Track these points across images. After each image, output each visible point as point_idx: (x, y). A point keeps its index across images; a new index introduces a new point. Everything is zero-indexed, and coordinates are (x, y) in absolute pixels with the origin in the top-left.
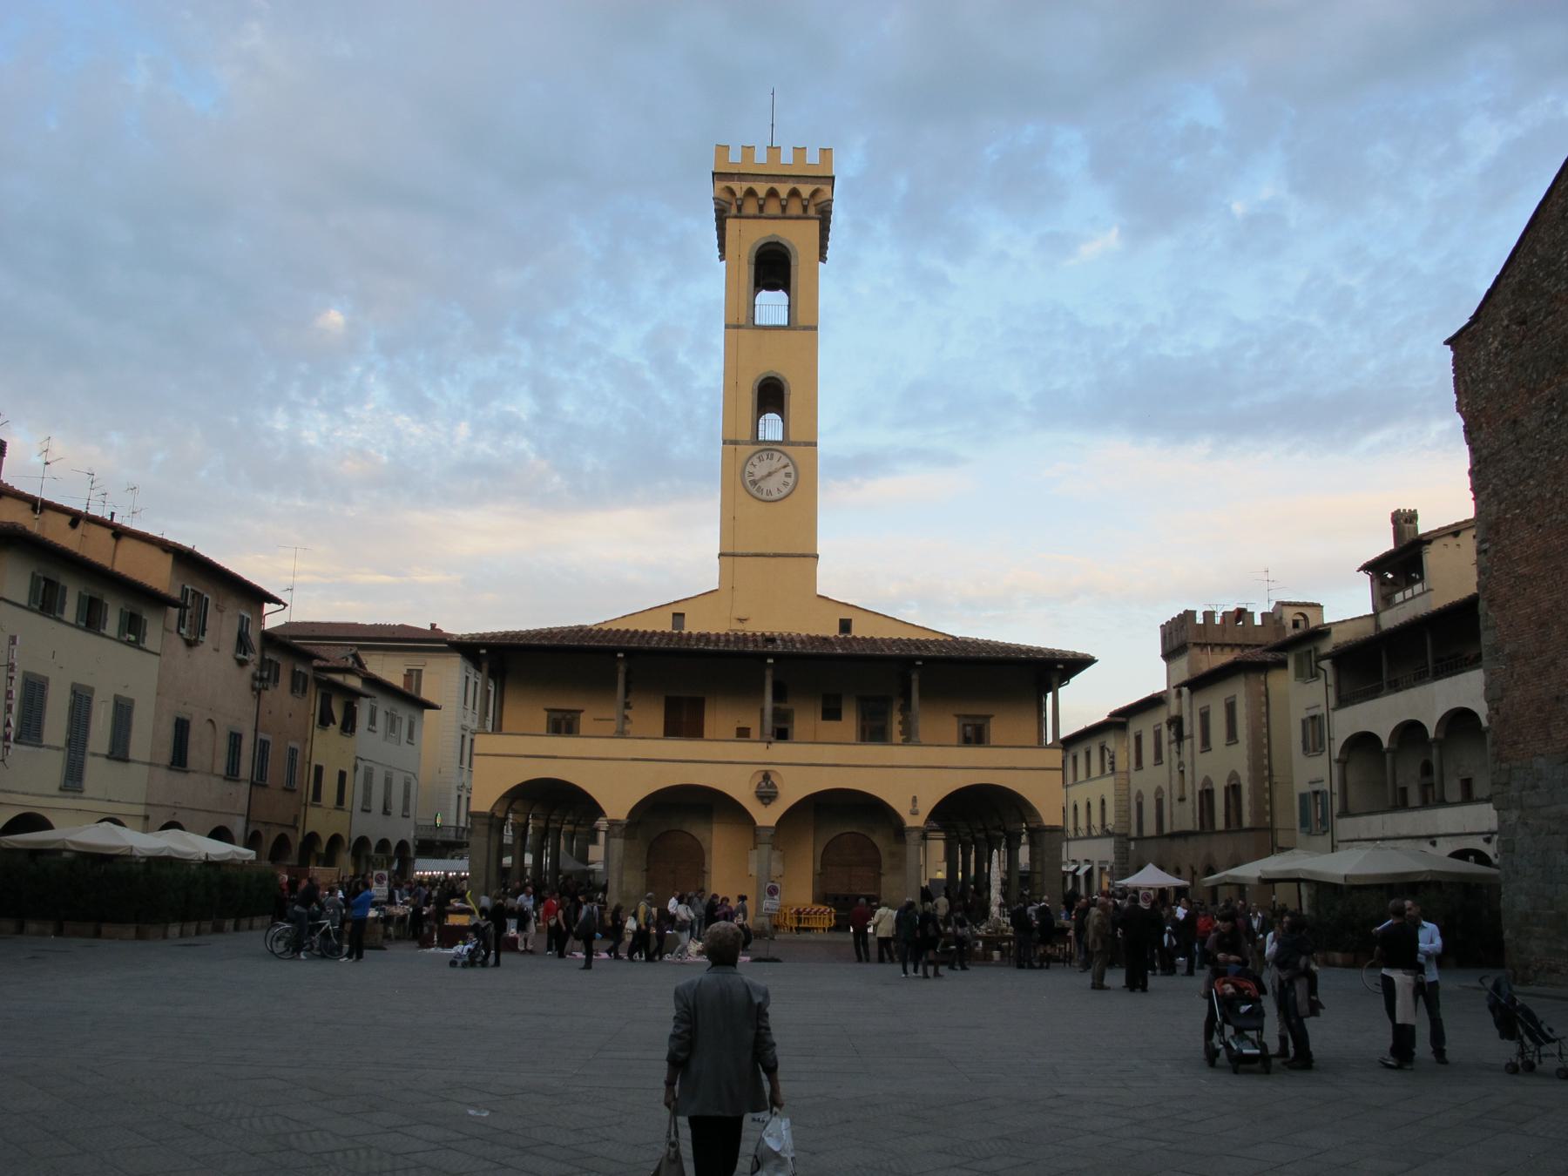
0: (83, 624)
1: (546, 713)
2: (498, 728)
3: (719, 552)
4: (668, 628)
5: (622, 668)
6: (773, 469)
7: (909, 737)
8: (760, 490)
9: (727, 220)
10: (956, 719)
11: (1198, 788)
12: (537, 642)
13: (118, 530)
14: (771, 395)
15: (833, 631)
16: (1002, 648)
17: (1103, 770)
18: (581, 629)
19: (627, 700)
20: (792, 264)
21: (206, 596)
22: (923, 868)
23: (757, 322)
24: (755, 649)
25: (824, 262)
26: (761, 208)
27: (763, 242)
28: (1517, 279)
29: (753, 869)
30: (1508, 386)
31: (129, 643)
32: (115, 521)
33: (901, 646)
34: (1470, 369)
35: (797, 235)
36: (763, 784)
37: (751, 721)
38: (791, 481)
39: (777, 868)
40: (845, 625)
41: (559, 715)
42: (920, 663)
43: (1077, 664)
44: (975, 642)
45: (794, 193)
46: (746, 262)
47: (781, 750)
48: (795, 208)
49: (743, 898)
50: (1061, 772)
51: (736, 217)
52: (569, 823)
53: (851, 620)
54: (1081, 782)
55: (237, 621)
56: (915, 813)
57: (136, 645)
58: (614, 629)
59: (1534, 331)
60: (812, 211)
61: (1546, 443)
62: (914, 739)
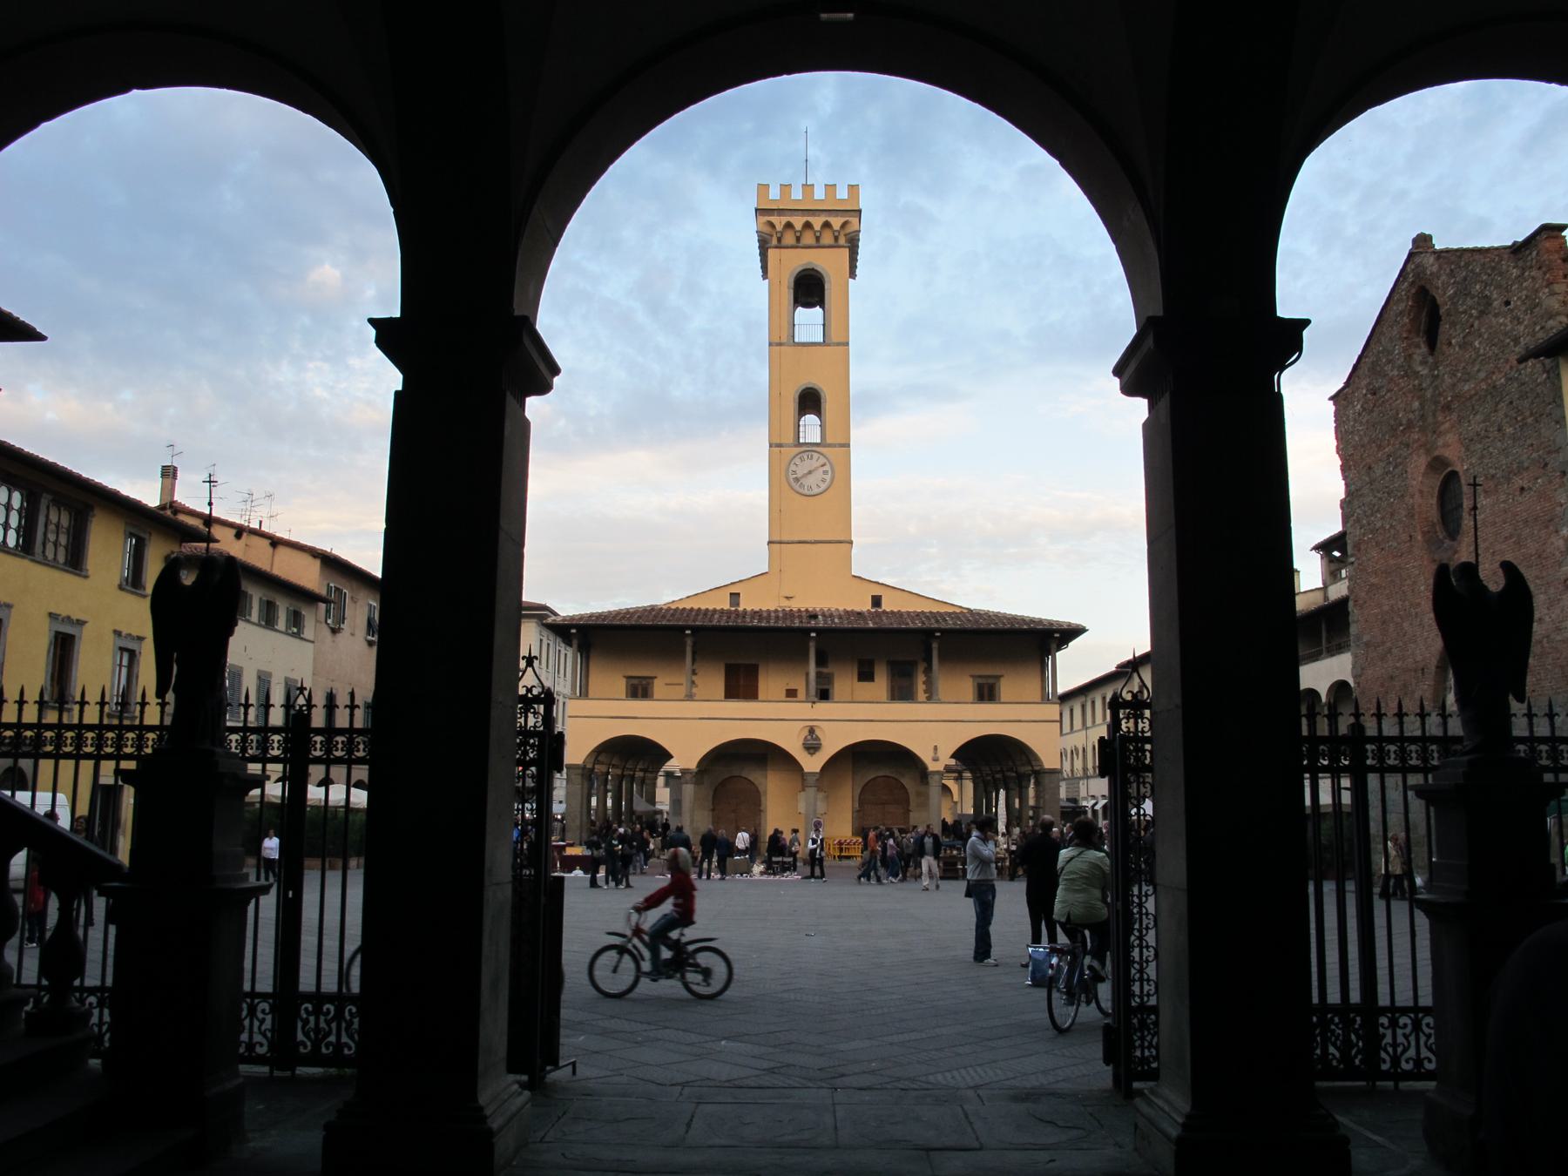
0: (263, 623)
2: (584, 694)
3: (768, 540)
4: (727, 606)
5: (689, 642)
6: (813, 468)
7: (931, 697)
8: (802, 486)
9: (769, 250)
10: (971, 679)
12: (618, 623)
13: (275, 540)
14: (809, 289)
15: (866, 606)
16: (1009, 619)
17: (1094, 722)
18: (652, 608)
19: (694, 667)
20: (826, 287)
21: (345, 591)
22: (959, 805)
23: (796, 340)
24: (801, 625)
25: (854, 279)
26: (798, 239)
27: (801, 269)
28: (1371, 360)
29: (802, 807)
30: (1366, 440)
31: (294, 635)
32: (263, 529)
33: (924, 619)
34: (1344, 422)
35: (828, 262)
36: (809, 737)
37: (798, 684)
38: (828, 477)
39: (821, 807)
40: (877, 601)
41: (635, 682)
42: (938, 634)
43: (1068, 634)
44: (987, 613)
45: (827, 225)
46: (786, 287)
47: (823, 709)
48: (827, 238)
49: (795, 831)
50: (1058, 724)
51: (776, 247)
52: (641, 770)
53: (881, 596)
54: (1099, 725)
55: (366, 609)
56: (936, 759)
57: (298, 635)
58: (681, 608)
59: (1380, 402)
60: (842, 241)
61: (1386, 487)
62: (935, 697)
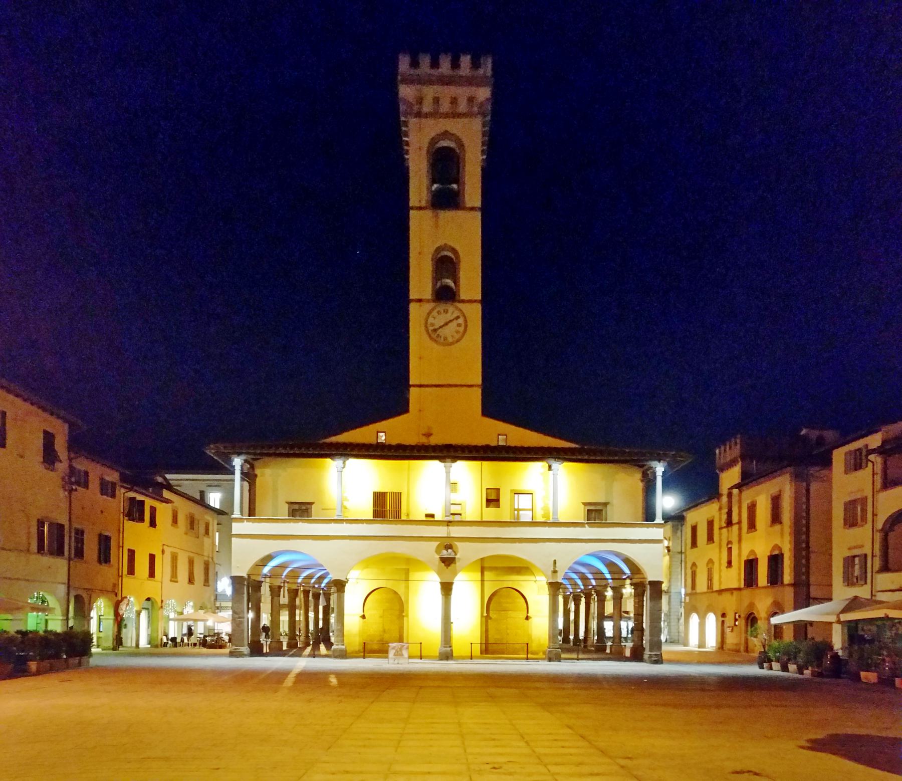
1: (287, 505)
11: (744, 557)
